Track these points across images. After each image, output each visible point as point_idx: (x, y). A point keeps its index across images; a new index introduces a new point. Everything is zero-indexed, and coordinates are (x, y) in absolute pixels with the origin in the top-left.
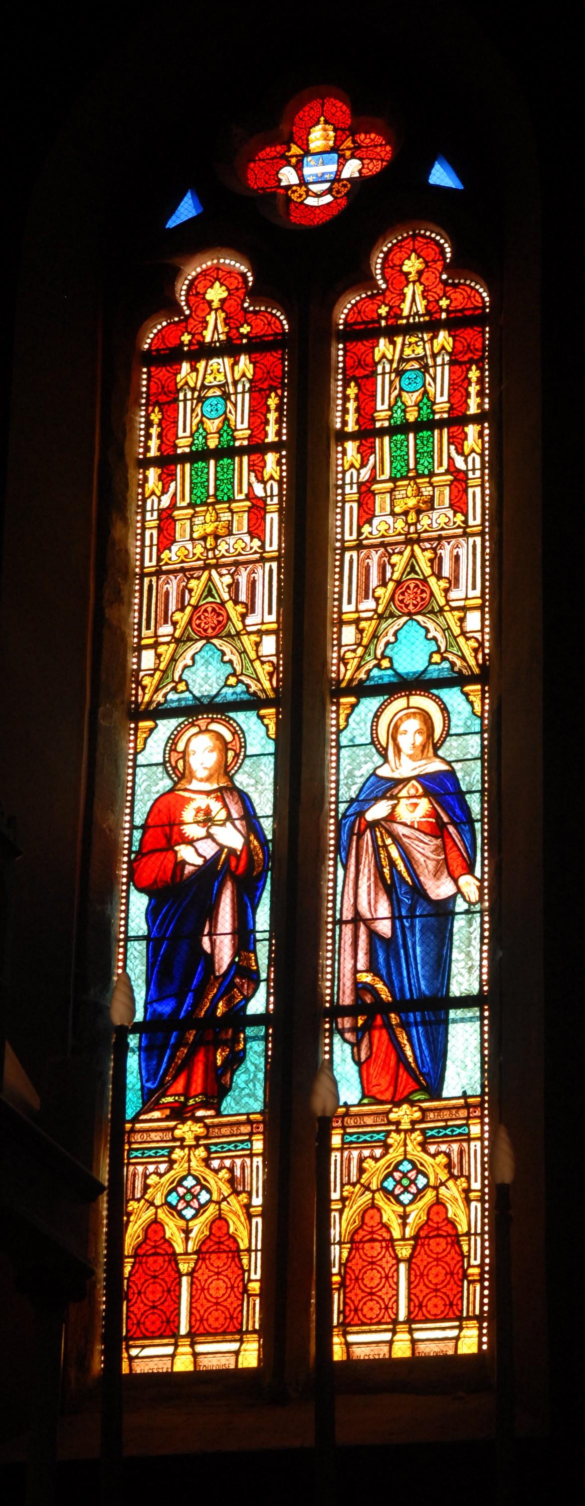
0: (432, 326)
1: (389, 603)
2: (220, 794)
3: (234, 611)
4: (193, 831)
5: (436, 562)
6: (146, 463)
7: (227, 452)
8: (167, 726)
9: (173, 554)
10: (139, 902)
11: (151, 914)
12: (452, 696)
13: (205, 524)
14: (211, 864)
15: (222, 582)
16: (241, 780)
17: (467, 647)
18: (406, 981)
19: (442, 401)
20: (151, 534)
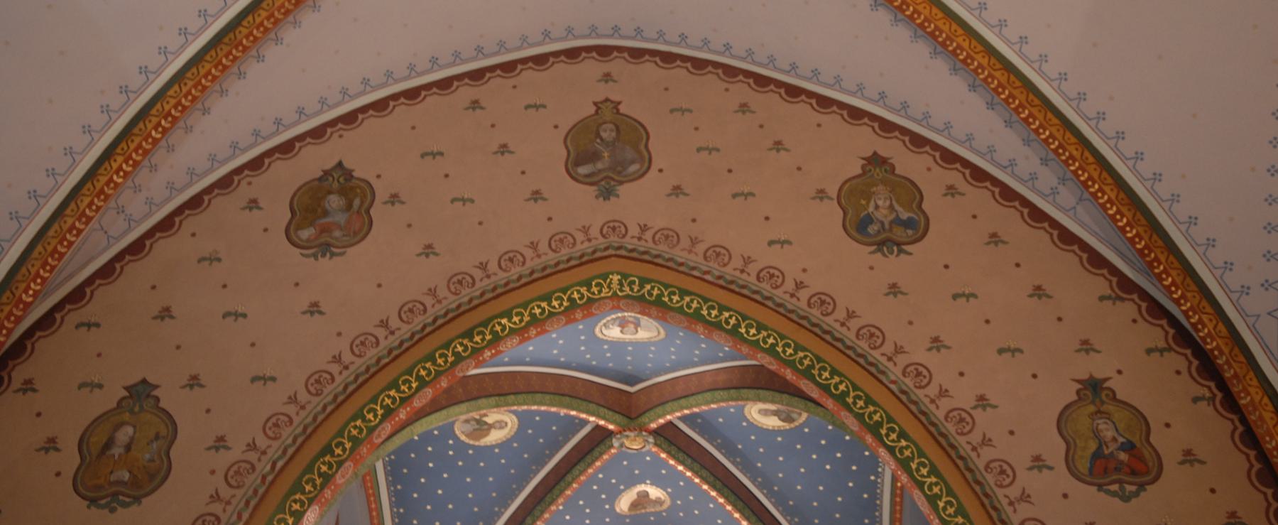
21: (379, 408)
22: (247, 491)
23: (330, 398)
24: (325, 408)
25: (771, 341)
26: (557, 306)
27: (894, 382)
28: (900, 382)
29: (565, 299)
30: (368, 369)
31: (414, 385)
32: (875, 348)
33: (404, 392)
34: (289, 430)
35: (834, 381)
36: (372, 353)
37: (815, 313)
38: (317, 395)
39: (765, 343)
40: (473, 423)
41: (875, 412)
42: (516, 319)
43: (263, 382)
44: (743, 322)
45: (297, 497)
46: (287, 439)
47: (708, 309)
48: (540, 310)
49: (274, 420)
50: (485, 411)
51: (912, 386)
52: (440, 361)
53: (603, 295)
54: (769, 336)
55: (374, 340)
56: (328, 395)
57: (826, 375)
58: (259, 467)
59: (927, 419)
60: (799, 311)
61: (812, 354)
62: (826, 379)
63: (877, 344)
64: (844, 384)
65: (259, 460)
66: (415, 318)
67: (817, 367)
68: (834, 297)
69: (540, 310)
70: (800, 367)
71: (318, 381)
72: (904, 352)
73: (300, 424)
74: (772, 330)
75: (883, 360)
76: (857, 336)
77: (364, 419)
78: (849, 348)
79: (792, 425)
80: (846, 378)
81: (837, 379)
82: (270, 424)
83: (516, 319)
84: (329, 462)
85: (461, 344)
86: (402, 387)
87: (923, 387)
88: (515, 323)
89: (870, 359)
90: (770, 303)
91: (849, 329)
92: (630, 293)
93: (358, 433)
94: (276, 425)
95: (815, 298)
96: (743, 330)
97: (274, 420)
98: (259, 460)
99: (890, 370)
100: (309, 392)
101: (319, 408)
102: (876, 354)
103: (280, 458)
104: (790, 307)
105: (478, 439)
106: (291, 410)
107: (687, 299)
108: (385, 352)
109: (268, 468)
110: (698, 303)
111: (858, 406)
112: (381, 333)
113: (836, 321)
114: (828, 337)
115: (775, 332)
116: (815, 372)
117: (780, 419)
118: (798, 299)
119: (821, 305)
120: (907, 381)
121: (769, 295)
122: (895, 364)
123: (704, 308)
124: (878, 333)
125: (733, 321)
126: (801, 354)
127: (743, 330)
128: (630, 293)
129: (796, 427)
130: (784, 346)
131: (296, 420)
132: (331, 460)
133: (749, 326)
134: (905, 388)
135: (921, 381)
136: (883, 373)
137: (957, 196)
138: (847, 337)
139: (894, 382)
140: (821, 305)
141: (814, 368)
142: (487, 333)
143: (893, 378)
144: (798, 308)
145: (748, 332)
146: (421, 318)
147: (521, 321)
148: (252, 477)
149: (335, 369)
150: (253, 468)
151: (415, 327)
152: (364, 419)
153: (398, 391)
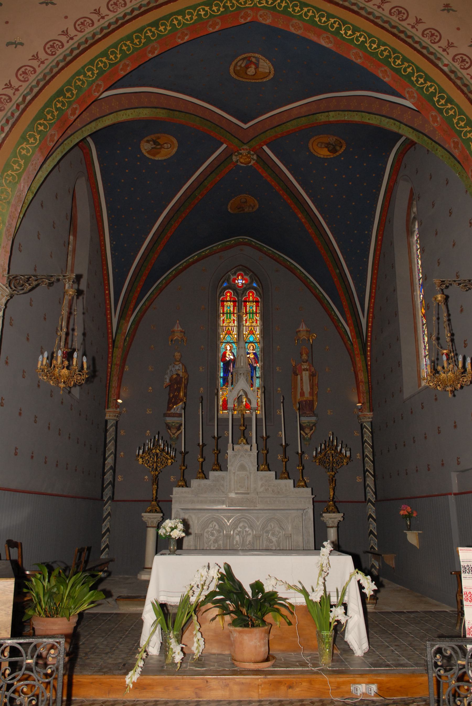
0: (253, 302)
1: (333, 645)
2: (231, 352)
3: (231, 332)
4: (228, 356)
5: (254, 329)
6: (221, 313)
7: (230, 313)
8: (224, 344)
9: (224, 324)
10: (222, 364)
11: (223, 365)
12: (256, 344)
13: (228, 321)
14: (230, 360)
15: (230, 328)
16: (233, 351)
17: (258, 339)
18: (258, 545)
19: (255, 310)
20: (222, 322)
21: (95, 69)
22: (7, 113)
23: (61, 57)
24: (58, 64)
25: (362, 39)
26: (216, 11)
27: (446, 65)
28: (451, 65)
29: (222, 5)
30: (86, 41)
31: (119, 56)
32: (434, 43)
33: (111, 60)
34: (34, 76)
35: (404, 66)
36: (89, 30)
37: (394, 19)
38: (52, 55)
39: (358, 41)
40: (151, 143)
41: (431, 86)
42: (188, 17)
43: (14, 46)
44: (344, 26)
45: (42, 121)
46: (32, 82)
47: (320, 17)
48: (204, 12)
49: (23, 69)
50: (159, 135)
51: (459, 68)
52: (136, 41)
53: (247, 5)
54: (360, 36)
55: (90, 22)
56: (59, 55)
57: (399, 62)
58: (14, 98)
59: (467, 89)
60: (383, 17)
61: (390, 47)
62: (399, 65)
63: (436, 41)
64: (411, 68)
65: (14, 94)
66: (118, 9)
67: (393, 56)
68: (408, 10)
69: (204, 12)
70: (381, 57)
71: (52, 46)
72: (453, 46)
73: (41, 72)
74: (363, 31)
75: (440, 50)
76: (423, 35)
77: (85, 75)
78: (417, 42)
79: (335, 155)
80: (413, 63)
81: (406, 64)
82: (20, 72)
83: (188, 17)
84: (62, 101)
85: (150, 31)
86: (111, 56)
87: (467, 69)
88: (187, 20)
89: (431, 50)
90: (363, 12)
91: (417, 30)
92: (266, 5)
93: (82, 84)
94: (24, 73)
95: (394, 10)
96: (343, 32)
97: (23, 69)
98: (14, 94)
99: (444, 57)
100: (46, 53)
101: (54, 63)
102: (435, 46)
103: (28, 94)
104: (377, 14)
105: (154, 155)
106: (35, 63)
107: (305, 9)
108: (98, 30)
109: (21, 99)
110: (313, 12)
111: (419, 83)
112: (95, 17)
113: (409, 24)
114: (402, 36)
115: (365, 32)
116: (391, 60)
117: (328, 150)
118: (383, 10)
119: (398, 14)
120: (456, 64)
121: (363, 6)
122: (448, 54)
123: (317, 16)
124: (436, 34)
125: (336, 26)
126: (382, 48)
127: (343, 32)
128: (266, 5)
129: (337, 156)
130: (370, 43)
131: (38, 70)
132: (63, 100)
133: (347, 29)
134: (453, 69)
135: (465, 65)
136: (439, 59)
137: (451, 12)
138: (416, 35)
139: (446, 65)
140: (398, 14)
141: (390, 58)
142: (168, 25)
143: (446, 62)
144: (383, 15)
145: (346, 33)
146: (122, 9)
147: (191, 19)
148: (10, 105)
149: (64, 39)
150: (10, 99)
151: (118, 14)
152: (85, 75)
153: (108, 58)
